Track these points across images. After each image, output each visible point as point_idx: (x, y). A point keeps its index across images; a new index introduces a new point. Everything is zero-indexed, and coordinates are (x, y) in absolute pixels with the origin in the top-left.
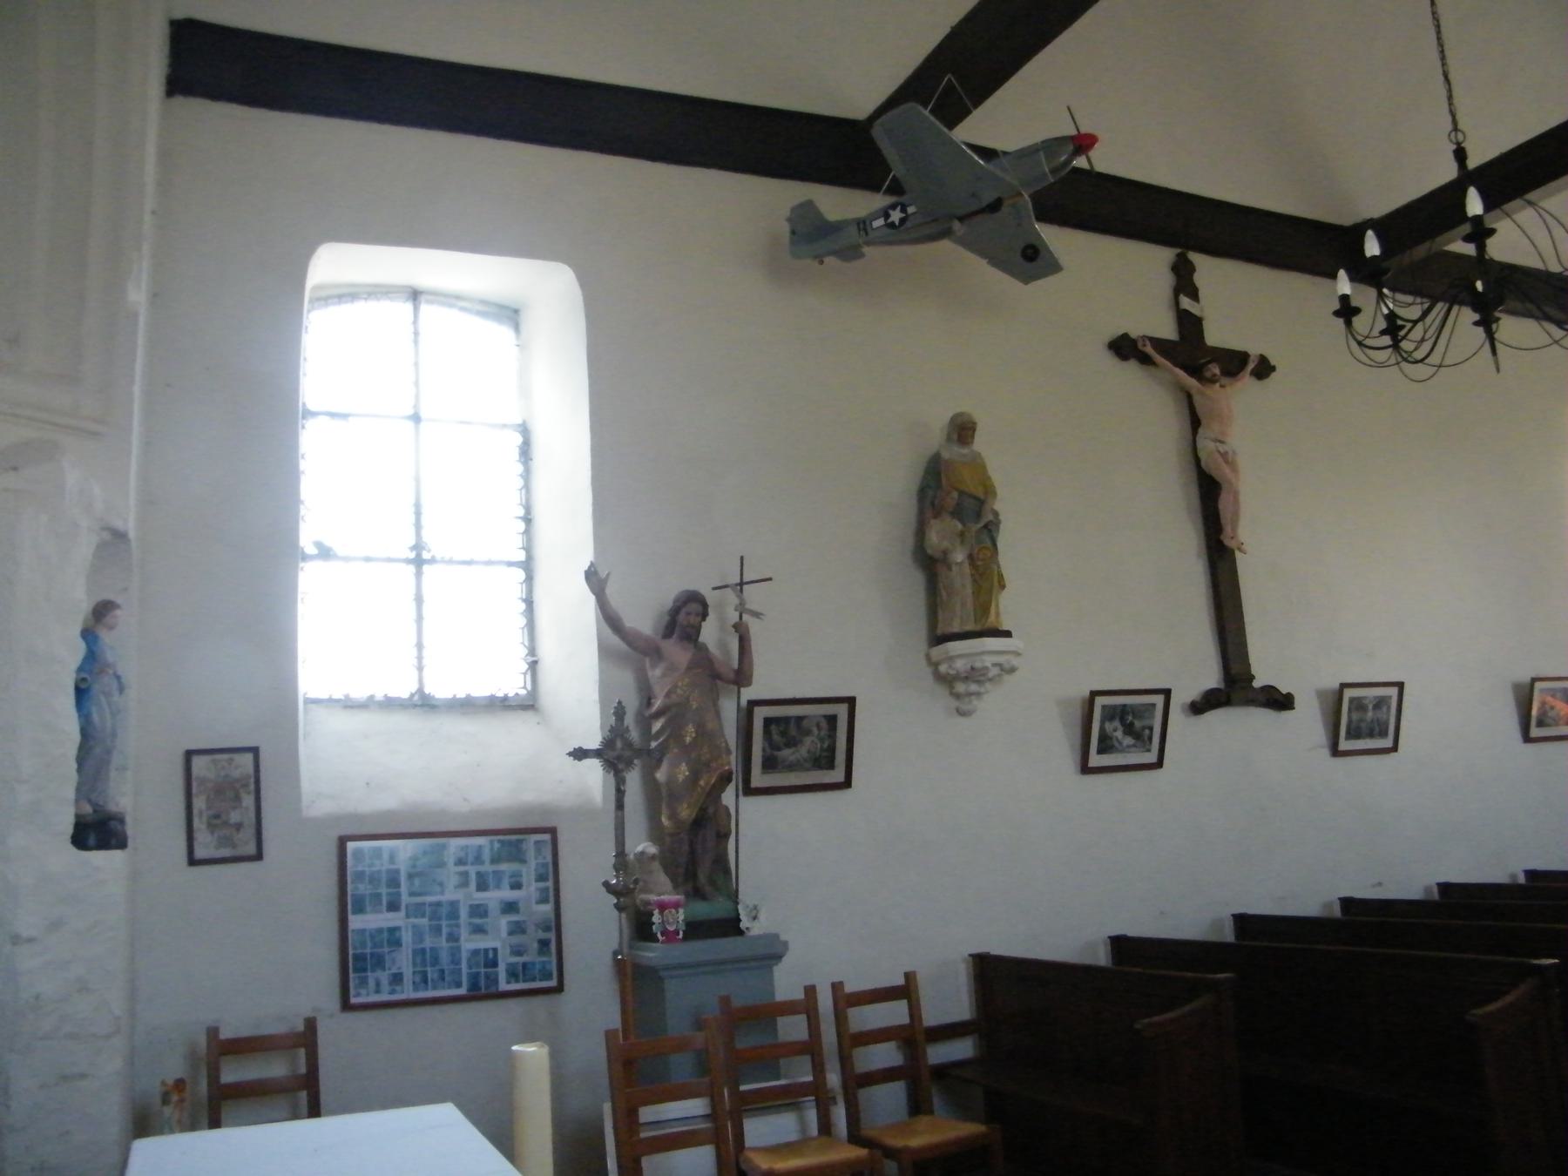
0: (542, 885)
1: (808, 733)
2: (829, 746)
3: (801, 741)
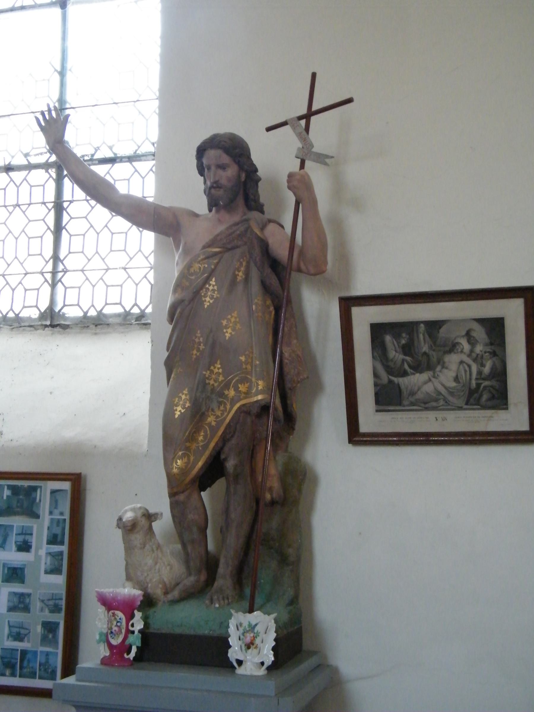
0: (56, 548)
1: (453, 347)
2: (493, 368)
3: (440, 361)
